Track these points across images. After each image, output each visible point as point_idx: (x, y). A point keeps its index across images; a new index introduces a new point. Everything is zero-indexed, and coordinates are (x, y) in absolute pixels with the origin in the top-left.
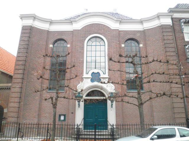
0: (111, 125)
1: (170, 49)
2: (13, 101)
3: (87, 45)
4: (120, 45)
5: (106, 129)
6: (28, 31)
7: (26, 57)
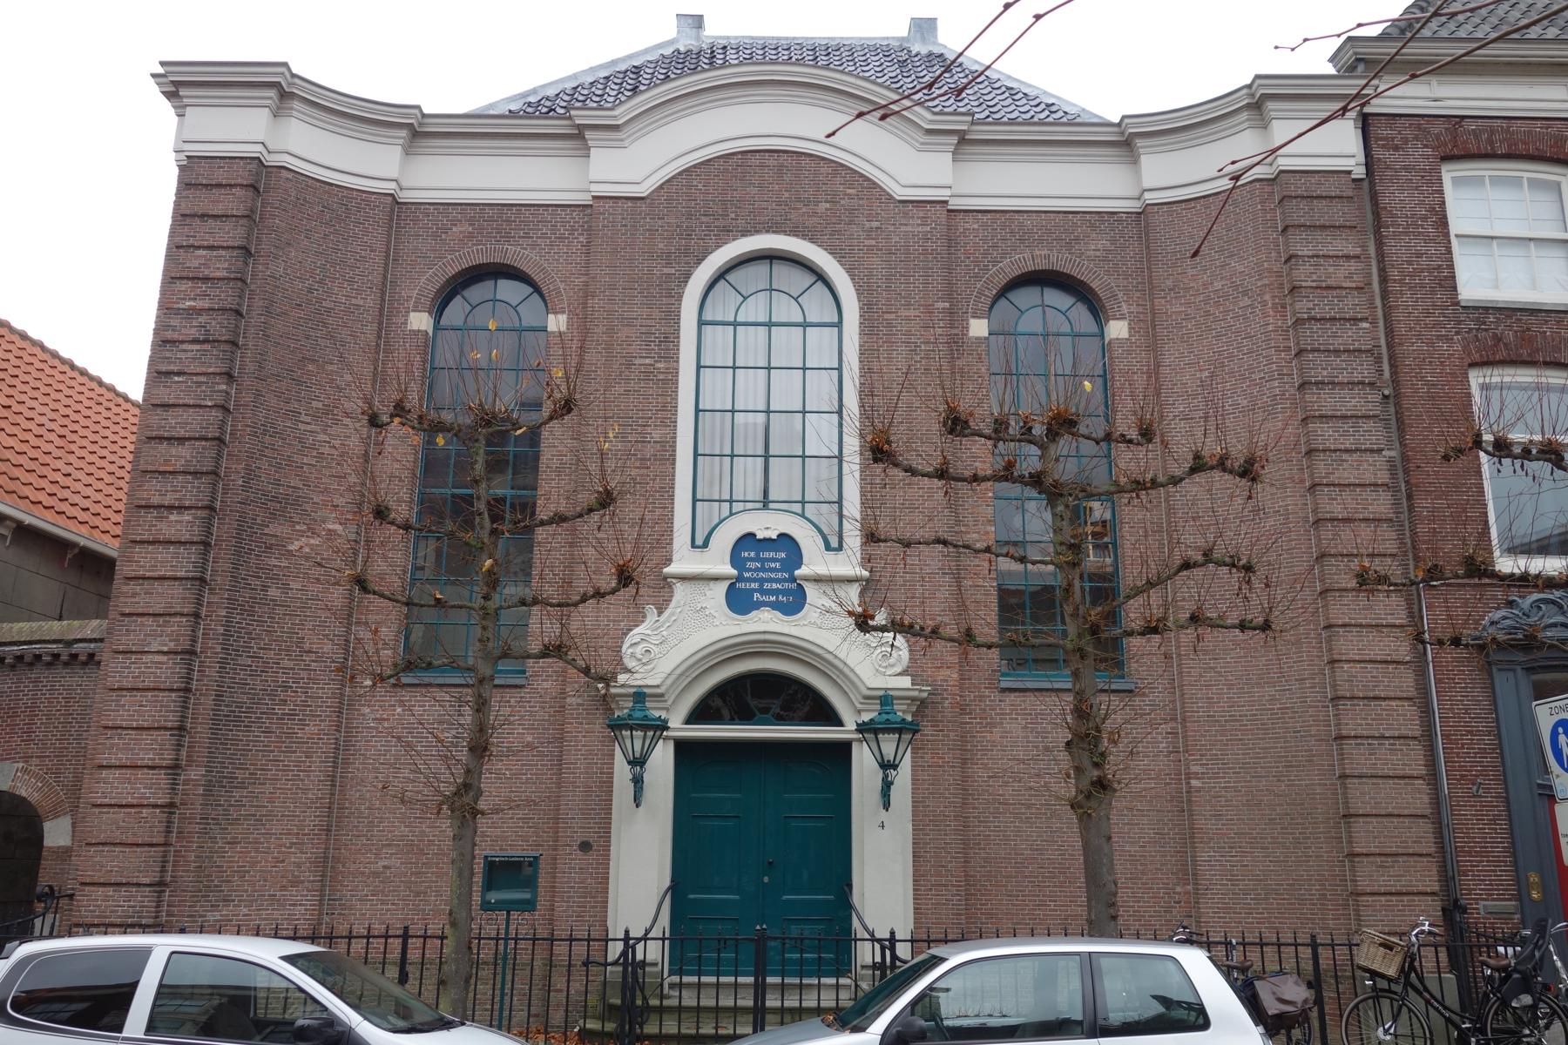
0: (873, 939)
1: (1338, 361)
2: (123, 757)
3: (701, 323)
4: (956, 319)
5: (841, 964)
6: (233, 202)
7: (226, 409)
